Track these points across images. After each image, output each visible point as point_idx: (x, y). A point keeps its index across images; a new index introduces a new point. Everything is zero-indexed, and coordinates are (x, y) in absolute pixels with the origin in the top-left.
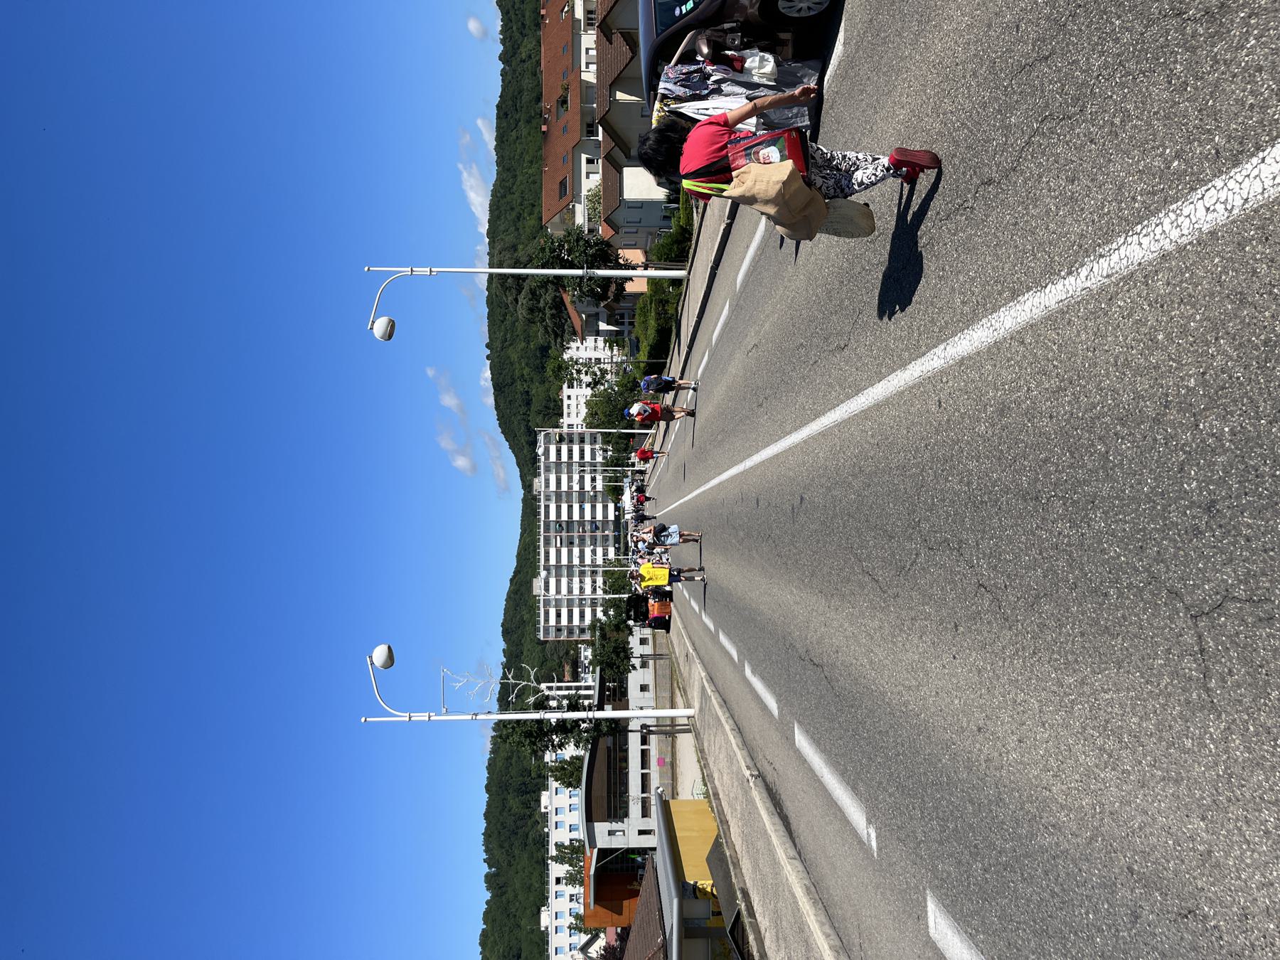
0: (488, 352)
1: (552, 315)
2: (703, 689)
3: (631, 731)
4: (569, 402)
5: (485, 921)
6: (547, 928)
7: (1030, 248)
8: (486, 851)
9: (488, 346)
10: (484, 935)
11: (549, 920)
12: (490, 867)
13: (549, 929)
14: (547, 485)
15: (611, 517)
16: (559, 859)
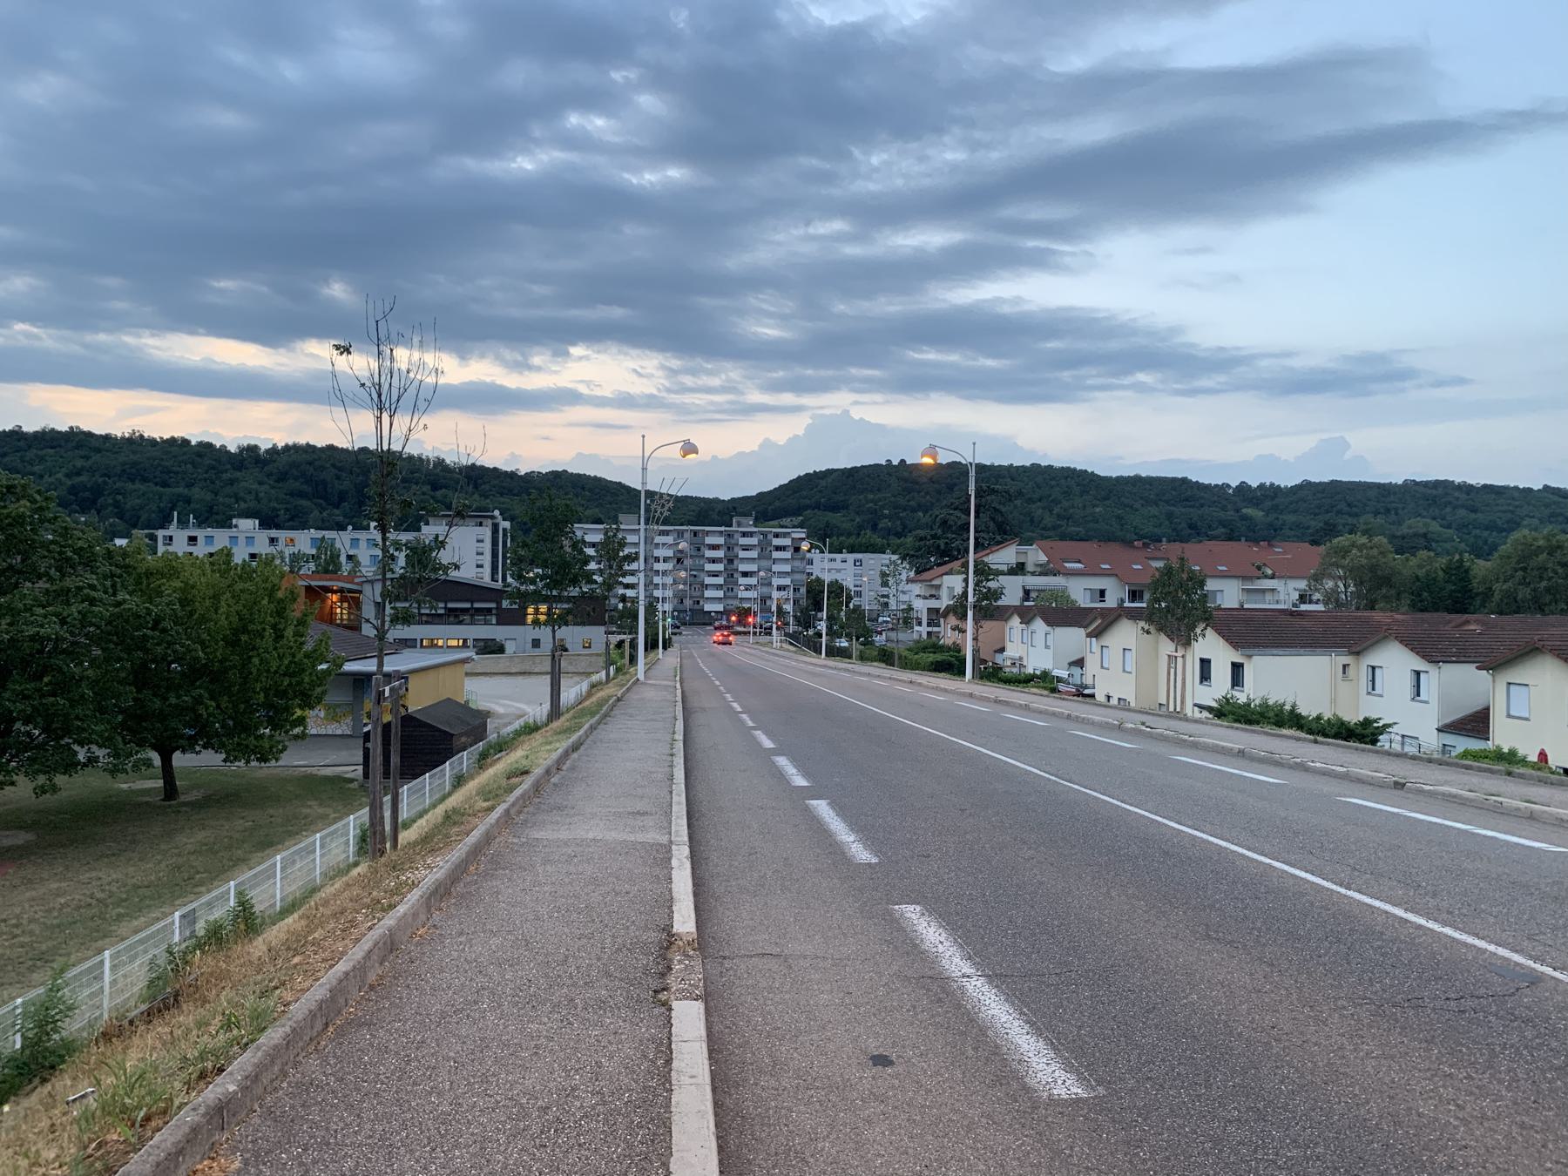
0: (1268, 484)
1: (939, 546)
2: (610, 697)
3: (554, 631)
4: (839, 561)
5: (200, 444)
6: (236, 526)
7: (463, 1032)
8: (287, 446)
9: (903, 461)
10: (186, 442)
11: (244, 529)
12: (267, 451)
13: (234, 530)
14: (744, 534)
15: (707, 607)
16: (320, 544)
